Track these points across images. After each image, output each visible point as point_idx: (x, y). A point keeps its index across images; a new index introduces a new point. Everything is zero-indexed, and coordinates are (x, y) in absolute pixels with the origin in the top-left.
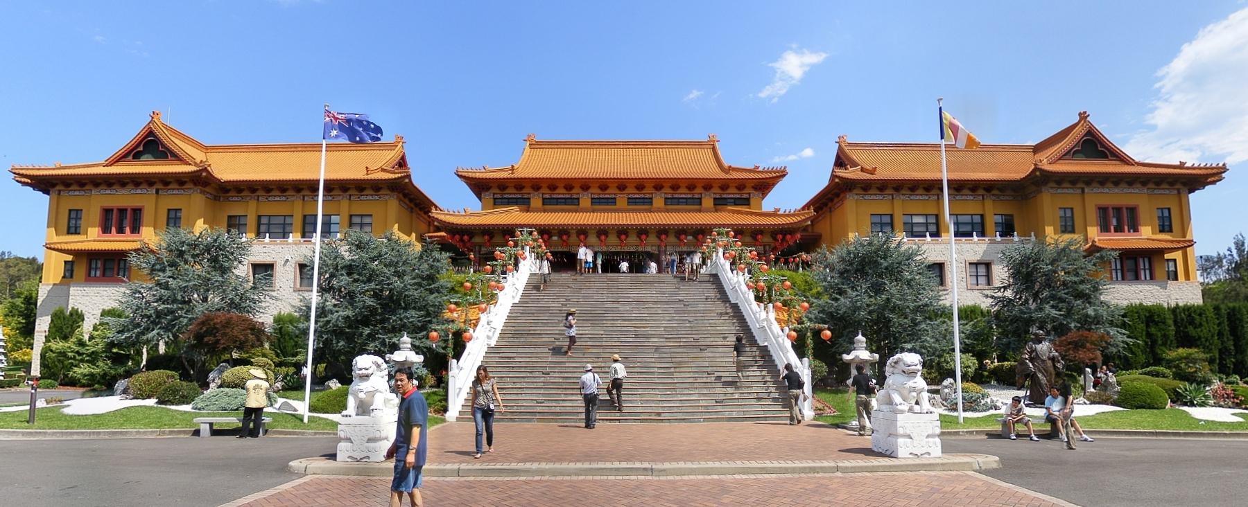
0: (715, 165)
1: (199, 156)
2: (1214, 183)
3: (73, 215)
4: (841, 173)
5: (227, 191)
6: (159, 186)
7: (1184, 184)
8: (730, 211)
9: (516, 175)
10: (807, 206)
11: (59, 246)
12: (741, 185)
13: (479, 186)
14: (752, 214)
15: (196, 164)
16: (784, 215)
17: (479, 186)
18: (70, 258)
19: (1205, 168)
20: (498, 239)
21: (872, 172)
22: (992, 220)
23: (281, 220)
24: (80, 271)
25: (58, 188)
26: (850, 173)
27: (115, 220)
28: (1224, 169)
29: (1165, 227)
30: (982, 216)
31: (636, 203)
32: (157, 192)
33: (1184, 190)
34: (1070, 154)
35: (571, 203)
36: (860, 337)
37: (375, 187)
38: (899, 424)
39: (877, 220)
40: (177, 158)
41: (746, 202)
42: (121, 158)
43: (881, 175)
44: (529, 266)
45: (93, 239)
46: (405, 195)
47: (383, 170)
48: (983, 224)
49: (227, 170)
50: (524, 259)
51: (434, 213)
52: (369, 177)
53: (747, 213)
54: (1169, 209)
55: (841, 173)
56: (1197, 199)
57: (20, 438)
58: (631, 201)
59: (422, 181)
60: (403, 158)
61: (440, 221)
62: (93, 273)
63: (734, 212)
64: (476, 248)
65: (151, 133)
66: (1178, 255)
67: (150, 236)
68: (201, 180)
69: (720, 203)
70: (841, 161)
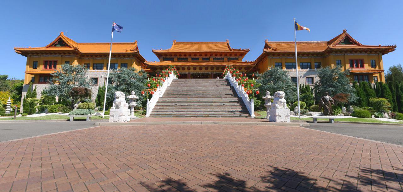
0: (228, 48)
1: (75, 46)
2: (392, 51)
3: (34, 63)
4: (266, 50)
5: (84, 56)
6: (63, 54)
7: (380, 52)
8: (232, 62)
9: (170, 52)
10: (159, 59)
11: (30, 72)
12: (236, 54)
13: (159, 55)
14: (239, 62)
15: (74, 48)
16: (248, 63)
17: (159, 55)
18: (33, 76)
19: (388, 46)
20: (159, 70)
21: (275, 50)
22: (314, 64)
23: (100, 65)
24: (37, 80)
25: (30, 54)
26: (269, 50)
27: (47, 64)
28: (395, 47)
29: (374, 66)
30: (311, 63)
31: (205, 60)
32: (62, 56)
33: (380, 54)
34: (339, 43)
35: (186, 60)
36: (268, 92)
37: (128, 55)
38: (277, 112)
39: (277, 64)
40: (71, 48)
41: (238, 59)
42: (50, 46)
43: (279, 50)
44: (173, 76)
45: (41, 70)
46: (137, 58)
47: (131, 50)
48: (311, 65)
49: (83, 50)
50: (171, 74)
51: (146, 62)
52: (127, 52)
53: (238, 62)
54: (341, 60)
55: (266, 50)
56: (384, 57)
57: (35, 122)
58: (203, 59)
59: (142, 54)
60: (137, 47)
61: (147, 65)
62: (41, 80)
63: (234, 62)
64: (155, 72)
65: (60, 38)
66: (378, 75)
67: (59, 68)
68: (76, 53)
69: (229, 60)
70: (266, 46)
